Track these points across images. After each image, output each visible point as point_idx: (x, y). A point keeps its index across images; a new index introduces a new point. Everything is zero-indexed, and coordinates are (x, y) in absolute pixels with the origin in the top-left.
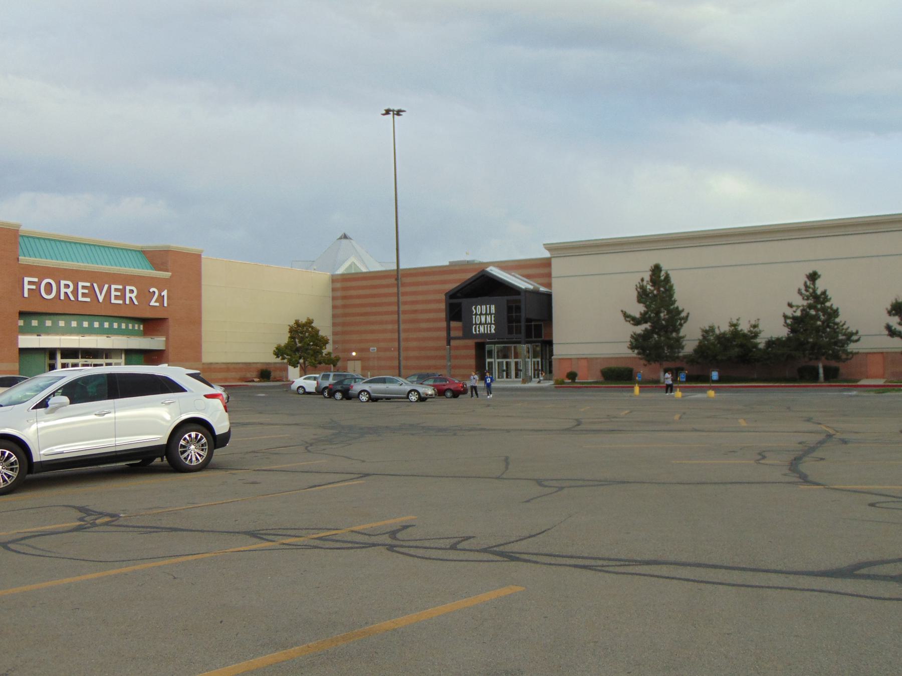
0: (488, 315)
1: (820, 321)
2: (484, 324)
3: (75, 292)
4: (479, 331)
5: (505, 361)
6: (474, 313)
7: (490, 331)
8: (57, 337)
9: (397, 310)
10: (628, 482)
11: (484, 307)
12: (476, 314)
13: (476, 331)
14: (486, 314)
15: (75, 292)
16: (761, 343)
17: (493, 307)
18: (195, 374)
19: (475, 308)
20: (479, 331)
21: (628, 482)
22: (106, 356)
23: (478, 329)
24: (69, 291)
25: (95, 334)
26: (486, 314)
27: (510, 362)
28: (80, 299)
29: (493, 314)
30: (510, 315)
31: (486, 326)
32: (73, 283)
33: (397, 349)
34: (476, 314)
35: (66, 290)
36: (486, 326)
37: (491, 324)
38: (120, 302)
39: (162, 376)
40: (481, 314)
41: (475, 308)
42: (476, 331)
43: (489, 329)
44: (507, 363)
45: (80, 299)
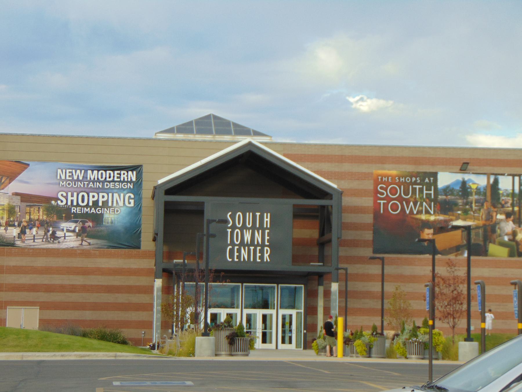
2: (248, 246)
3: (76, 211)
4: (239, 257)
5: (259, 313)
6: (229, 225)
9: (385, 267)
11: (249, 216)
15: (76, 211)
16: (498, 191)
17: (267, 219)
19: (233, 217)
20: (239, 257)
22: (271, 308)
23: (236, 254)
24: (75, 211)
25: (97, 239)
27: (255, 315)
28: (78, 212)
31: (252, 248)
32: (268, 247)
35: (74, 210)
36: (252, 248)
38: (80, 212)
41: (233, 217)
43: (258, 255)
44: (264, 317)
45: (78, 212)
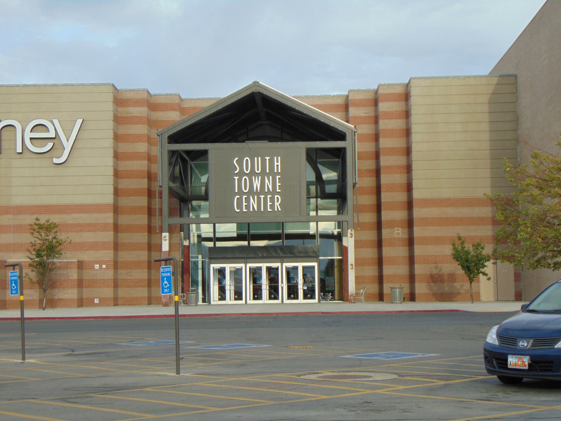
0: (268, 175)
1: (79, 274)
2: (258, 194)
4: (247, 207)
7: (272, 206)
8: (299, 290)
10: (108, 376)
11: (258, 161)
12: (241, 174)
13: (240, 205)
14: (263, 174)
17: (278, 163)
18: (506, 319)
19: (240, 163)
20: (247, 207)
21: (108, 376)
26: (263, 174)
29: (278, 173)
30: (12, 226)
33: (382, 190)
34: (241, 174)
37: (274, 192)
39: (243, 97)
40: (253, 173)
41: (240, 163)
42: (240, 205)
